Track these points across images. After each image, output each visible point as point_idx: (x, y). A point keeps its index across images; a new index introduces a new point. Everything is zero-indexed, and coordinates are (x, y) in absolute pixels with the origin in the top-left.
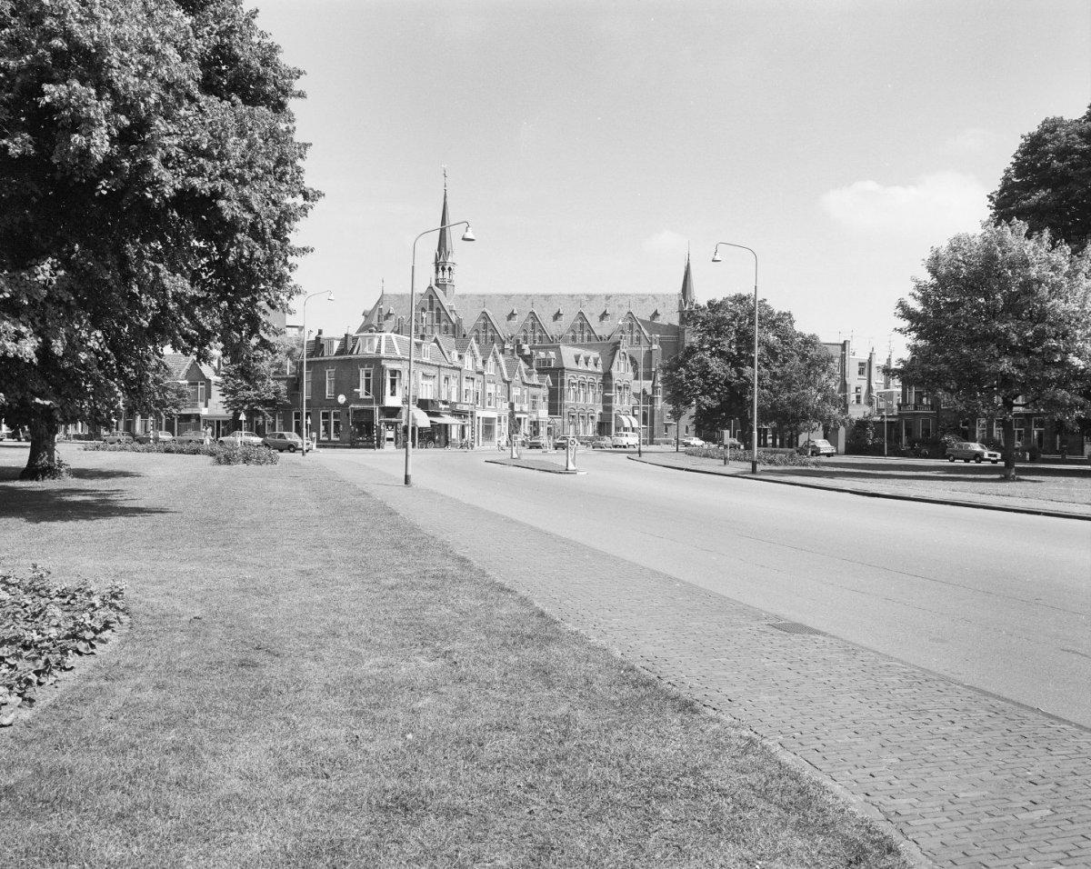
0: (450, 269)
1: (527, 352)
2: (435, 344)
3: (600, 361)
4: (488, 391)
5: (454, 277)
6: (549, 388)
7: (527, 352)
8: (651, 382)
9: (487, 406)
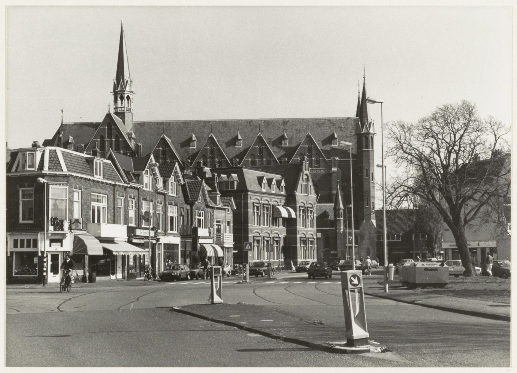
0: (128, 98)
1: (208, 175)
2: (109, 162)
3: (283, 184)
4: (170, 214)
5: (133, 106)
6: (233, 211)
7: (208, 175)
8: (333, 205)
9: (169, 232)
